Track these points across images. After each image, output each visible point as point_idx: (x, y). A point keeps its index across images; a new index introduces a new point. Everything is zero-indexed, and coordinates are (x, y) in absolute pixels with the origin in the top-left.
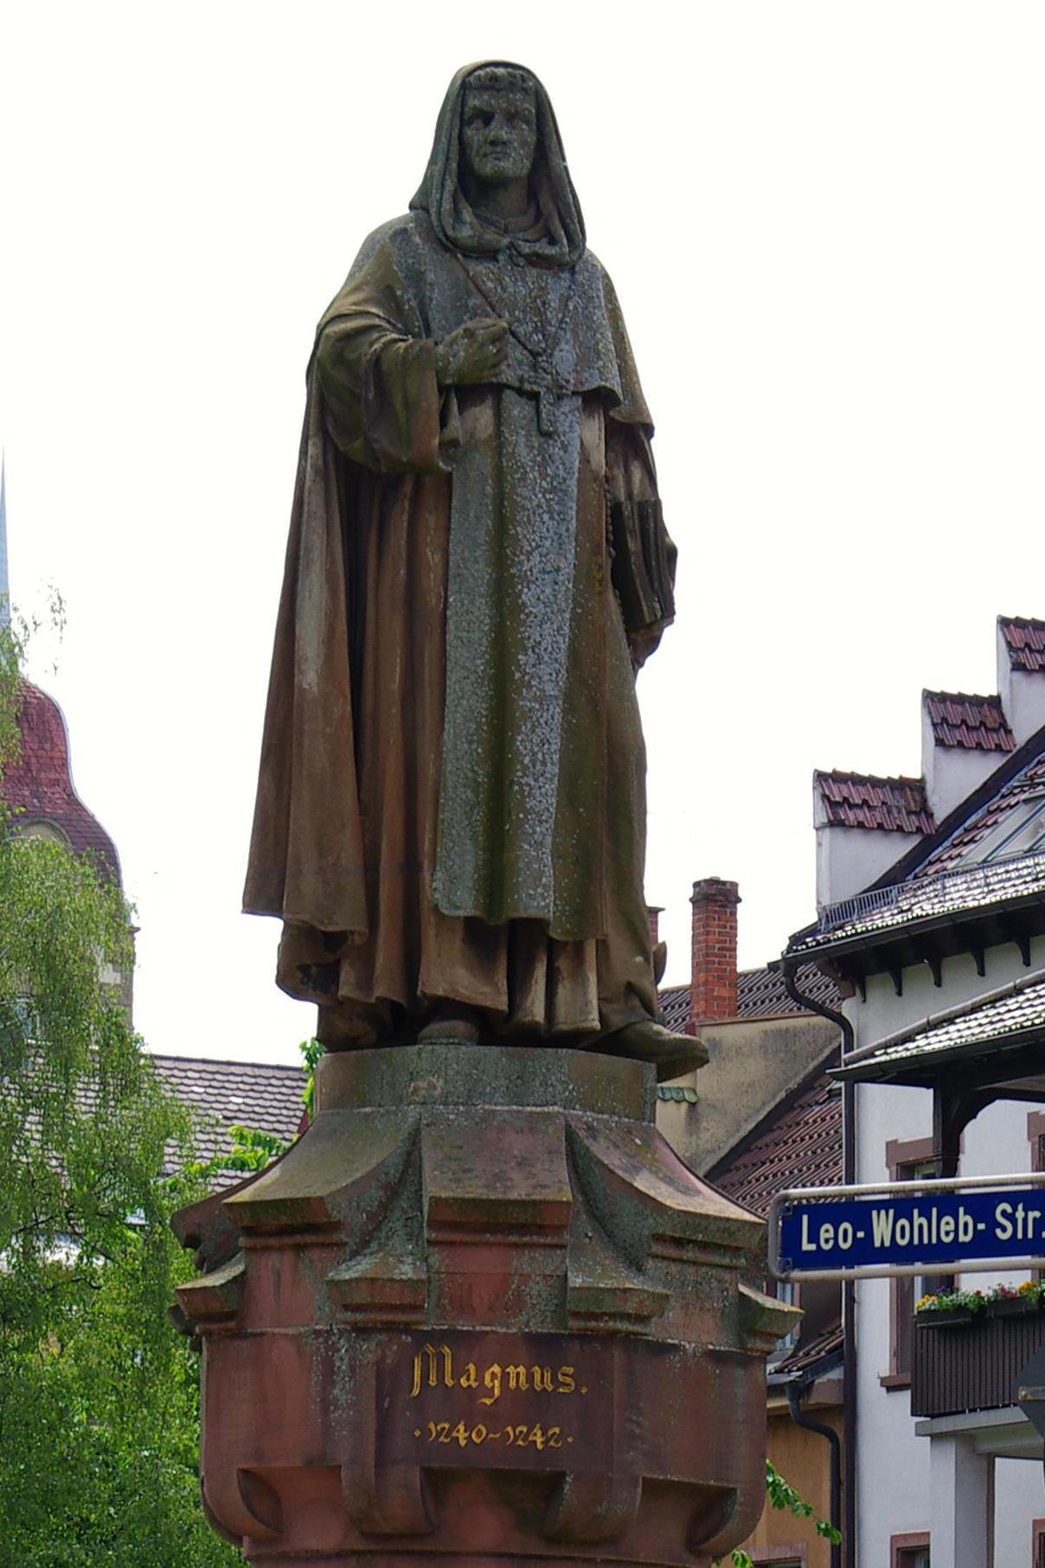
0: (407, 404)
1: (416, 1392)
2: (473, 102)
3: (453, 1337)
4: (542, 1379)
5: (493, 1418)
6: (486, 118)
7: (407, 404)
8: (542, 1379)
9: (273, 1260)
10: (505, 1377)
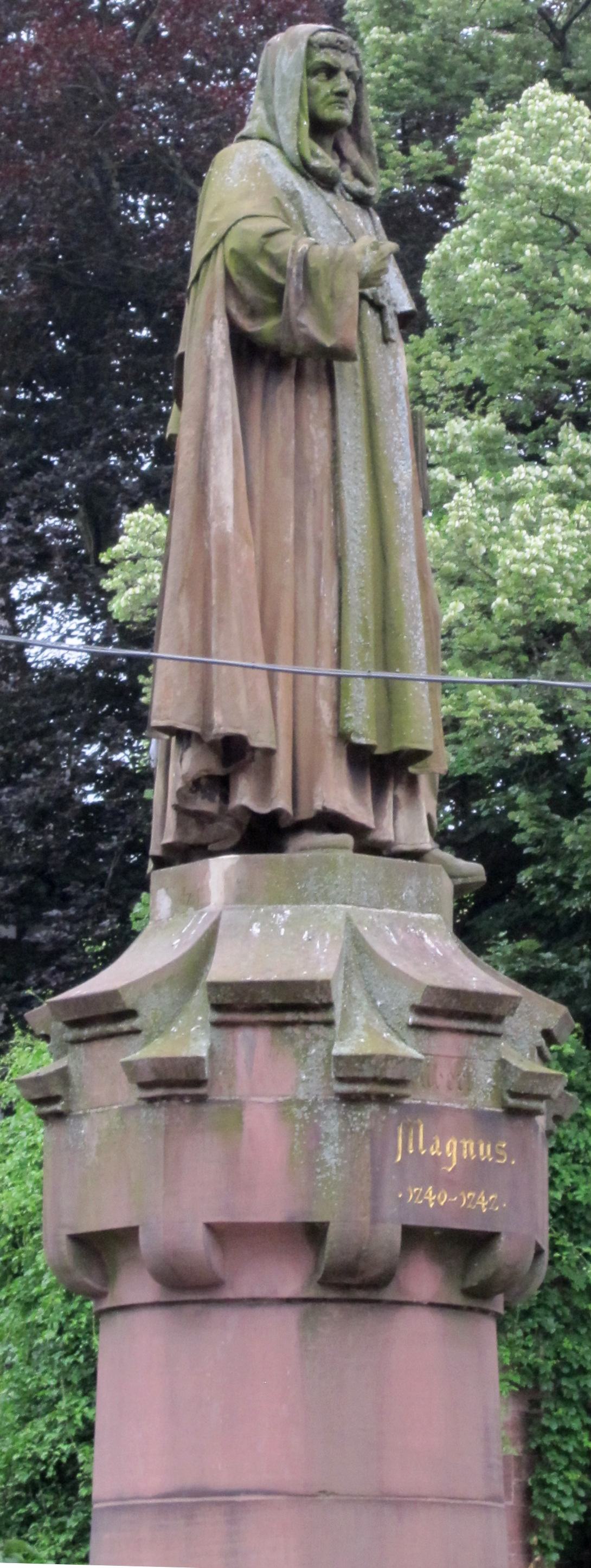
0: (332, 296)
1: (399, 1158)
2: (322, 57)
3: (424, 1110)
4: (485, 1151)
5: (451, 1184)
6: (331, 71)
7: (332, 296)
8: (485, 1151)
9: (242, 1035)
10: (460, 1147)
